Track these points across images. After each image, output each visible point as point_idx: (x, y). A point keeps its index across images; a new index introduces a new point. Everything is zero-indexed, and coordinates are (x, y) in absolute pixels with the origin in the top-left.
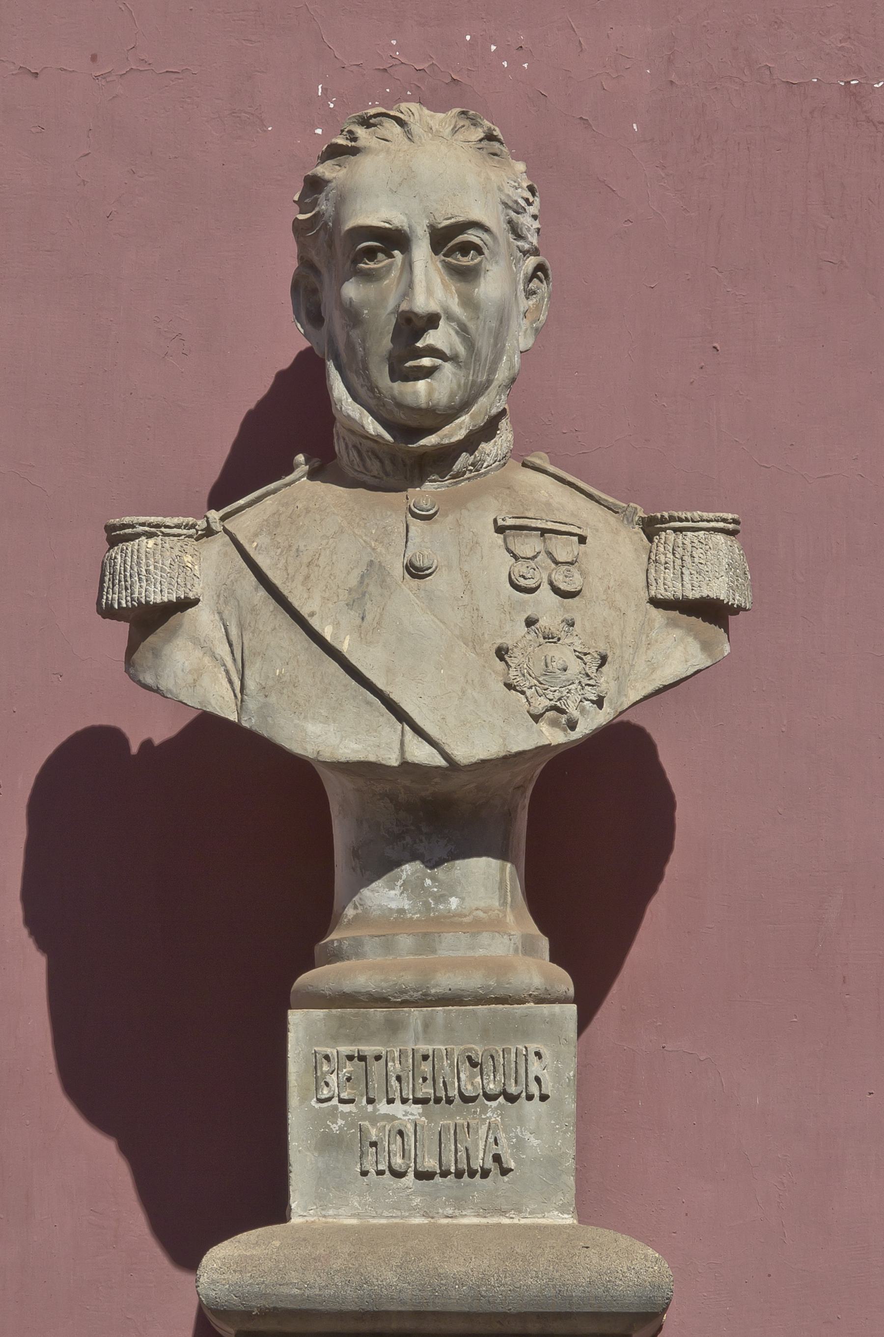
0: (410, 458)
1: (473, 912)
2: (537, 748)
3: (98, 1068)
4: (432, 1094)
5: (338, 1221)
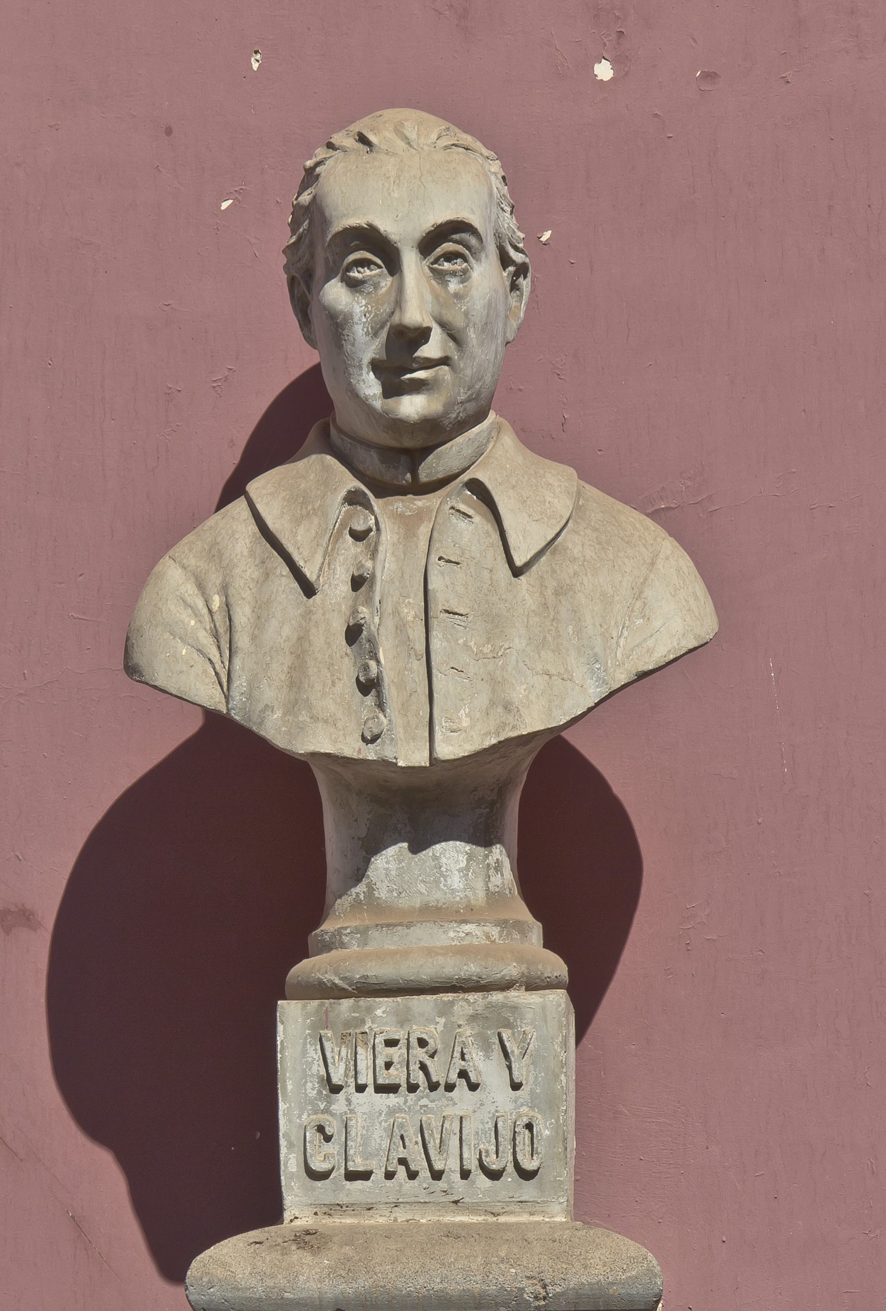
0: (398, 463)
1: (447, 895)
3: (97, 1080)
4: (418, 1065)
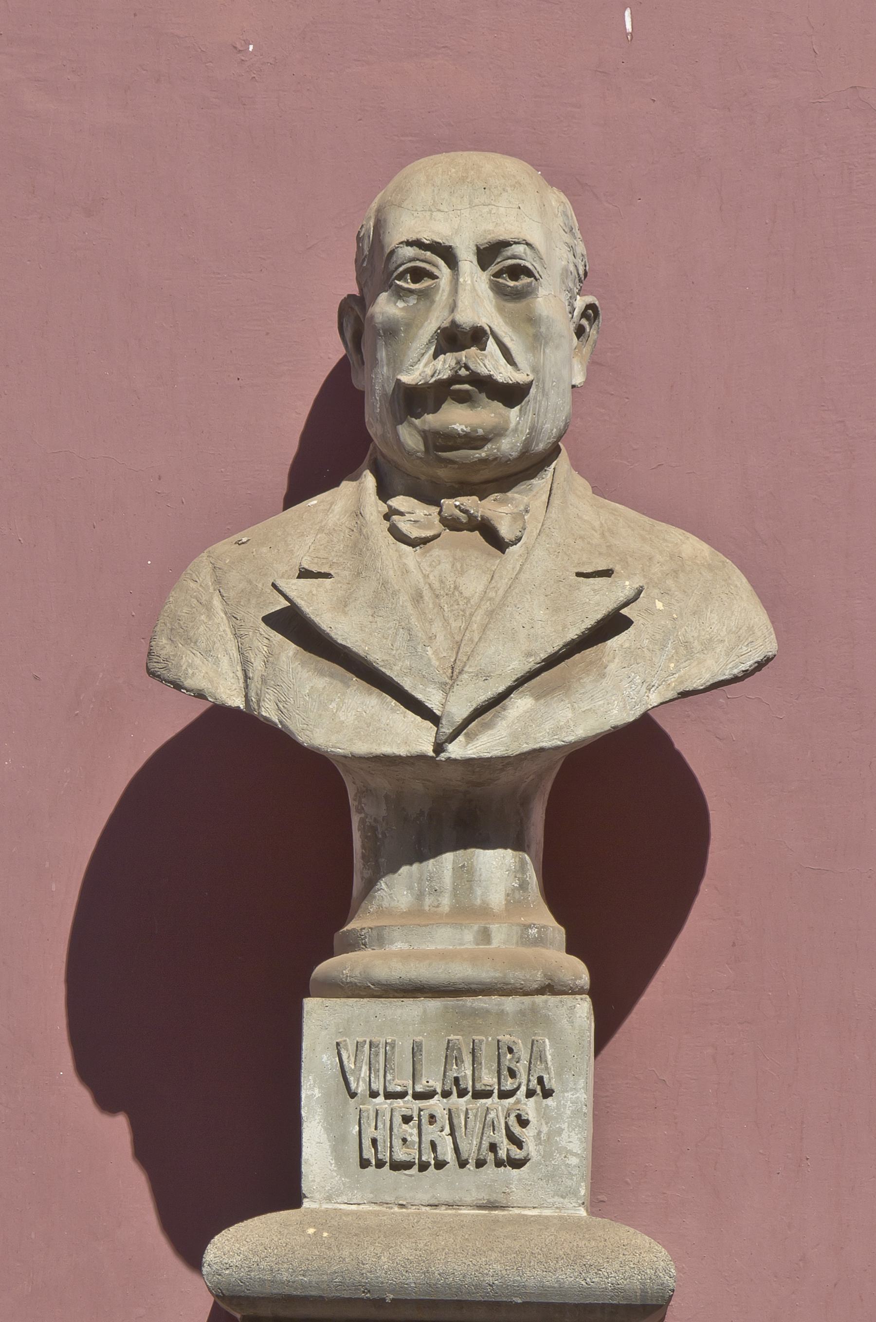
4: (436, 1060)
5: (339, 1210)
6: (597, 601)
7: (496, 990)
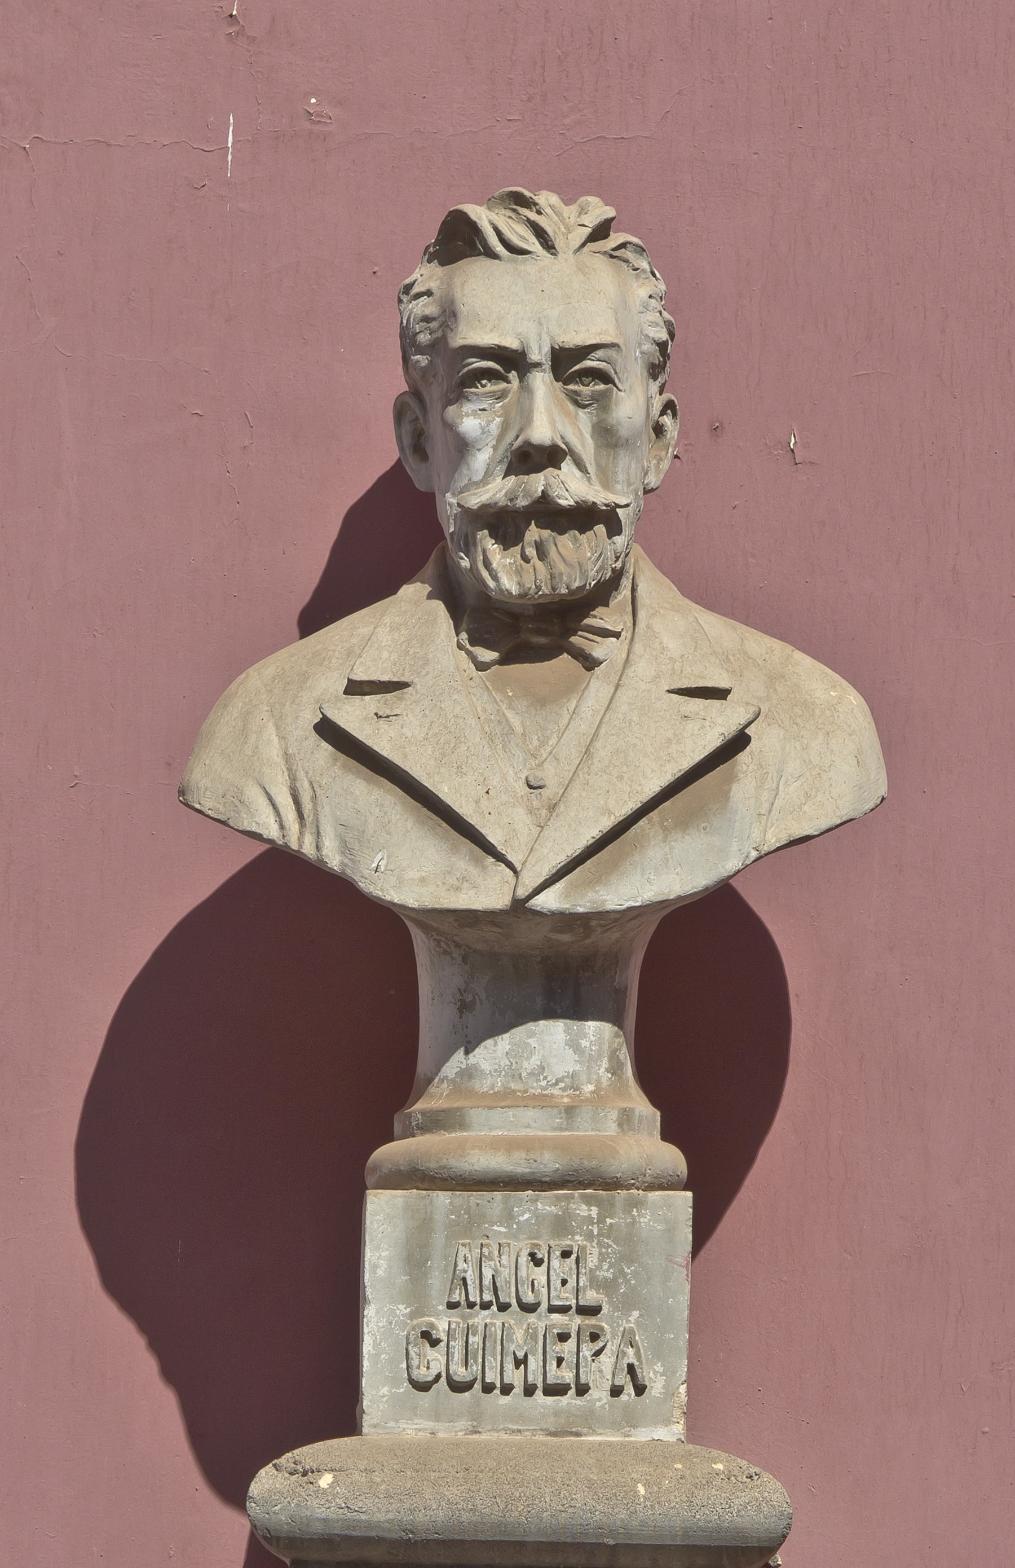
2: (389, 682)
4: (516, 1260)
5: (400, 1446)
6: (714, 725)
7: (569, 1181)
